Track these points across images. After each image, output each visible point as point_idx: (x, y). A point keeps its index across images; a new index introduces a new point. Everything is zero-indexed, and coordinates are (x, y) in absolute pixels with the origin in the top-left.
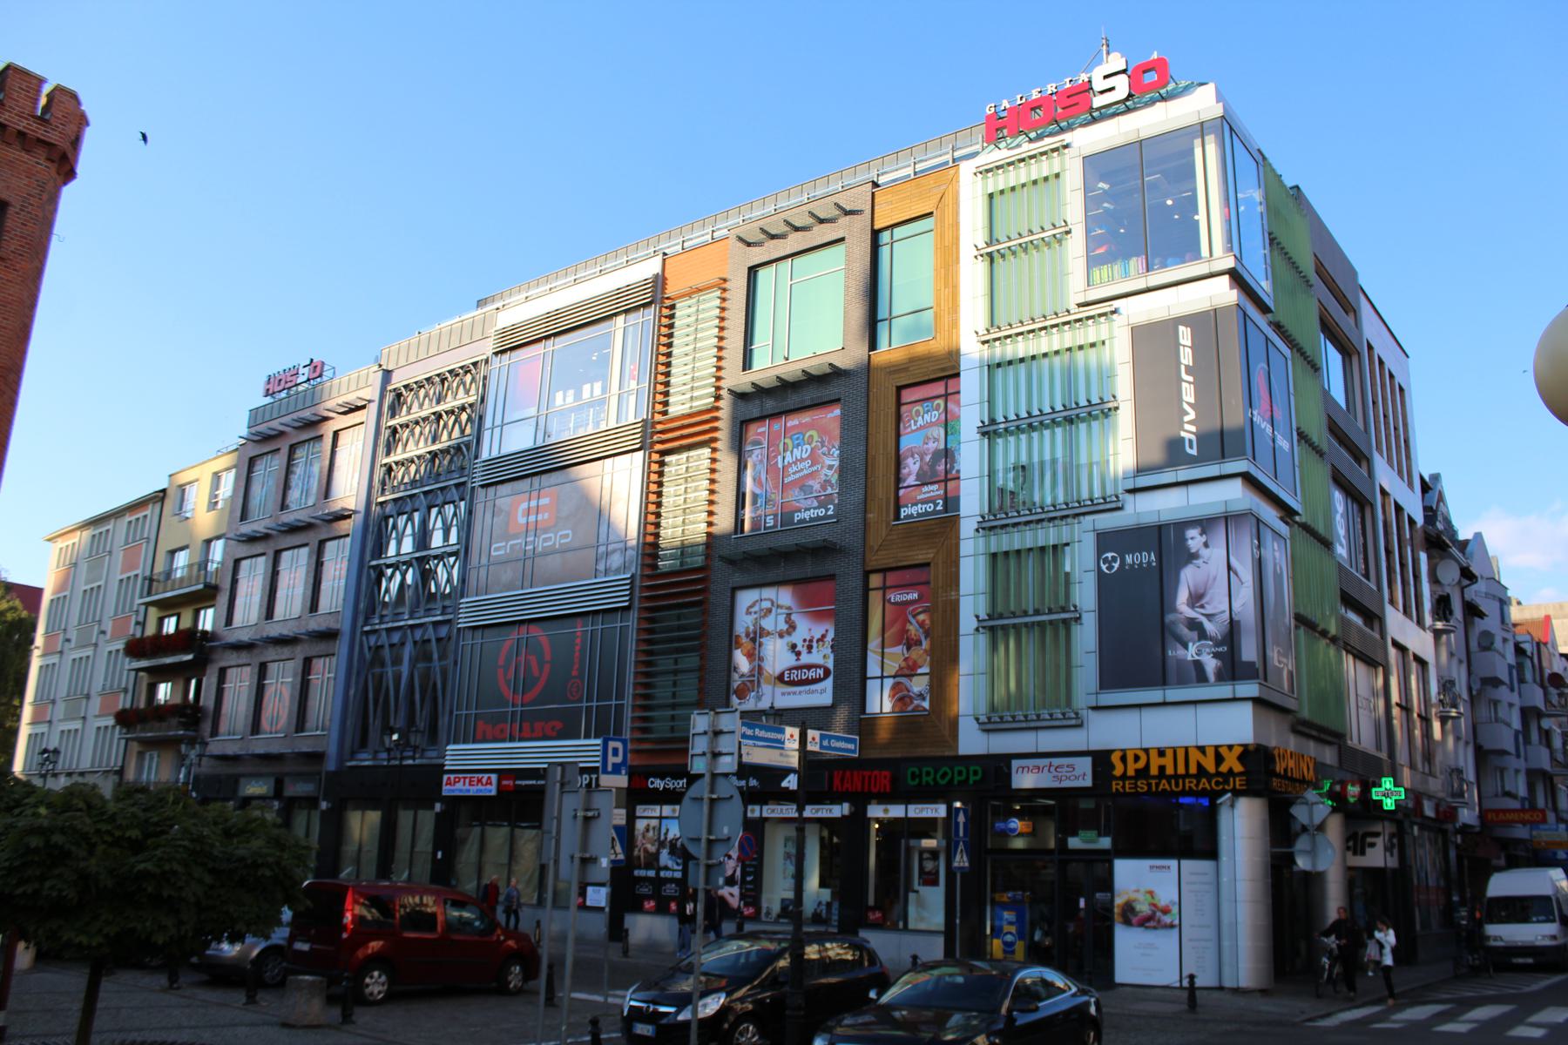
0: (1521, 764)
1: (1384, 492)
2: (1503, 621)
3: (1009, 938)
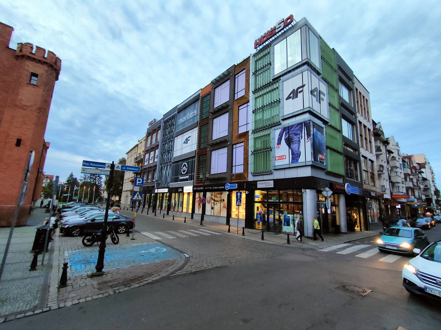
0: (404, 185)
1: (360, 123)
2: (398, 154)
3: (259, 221)
